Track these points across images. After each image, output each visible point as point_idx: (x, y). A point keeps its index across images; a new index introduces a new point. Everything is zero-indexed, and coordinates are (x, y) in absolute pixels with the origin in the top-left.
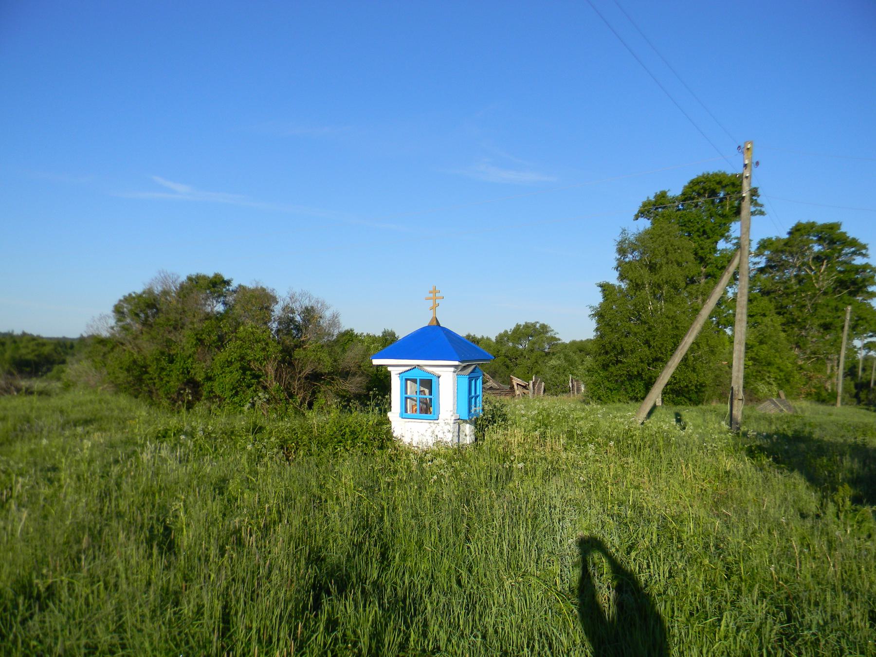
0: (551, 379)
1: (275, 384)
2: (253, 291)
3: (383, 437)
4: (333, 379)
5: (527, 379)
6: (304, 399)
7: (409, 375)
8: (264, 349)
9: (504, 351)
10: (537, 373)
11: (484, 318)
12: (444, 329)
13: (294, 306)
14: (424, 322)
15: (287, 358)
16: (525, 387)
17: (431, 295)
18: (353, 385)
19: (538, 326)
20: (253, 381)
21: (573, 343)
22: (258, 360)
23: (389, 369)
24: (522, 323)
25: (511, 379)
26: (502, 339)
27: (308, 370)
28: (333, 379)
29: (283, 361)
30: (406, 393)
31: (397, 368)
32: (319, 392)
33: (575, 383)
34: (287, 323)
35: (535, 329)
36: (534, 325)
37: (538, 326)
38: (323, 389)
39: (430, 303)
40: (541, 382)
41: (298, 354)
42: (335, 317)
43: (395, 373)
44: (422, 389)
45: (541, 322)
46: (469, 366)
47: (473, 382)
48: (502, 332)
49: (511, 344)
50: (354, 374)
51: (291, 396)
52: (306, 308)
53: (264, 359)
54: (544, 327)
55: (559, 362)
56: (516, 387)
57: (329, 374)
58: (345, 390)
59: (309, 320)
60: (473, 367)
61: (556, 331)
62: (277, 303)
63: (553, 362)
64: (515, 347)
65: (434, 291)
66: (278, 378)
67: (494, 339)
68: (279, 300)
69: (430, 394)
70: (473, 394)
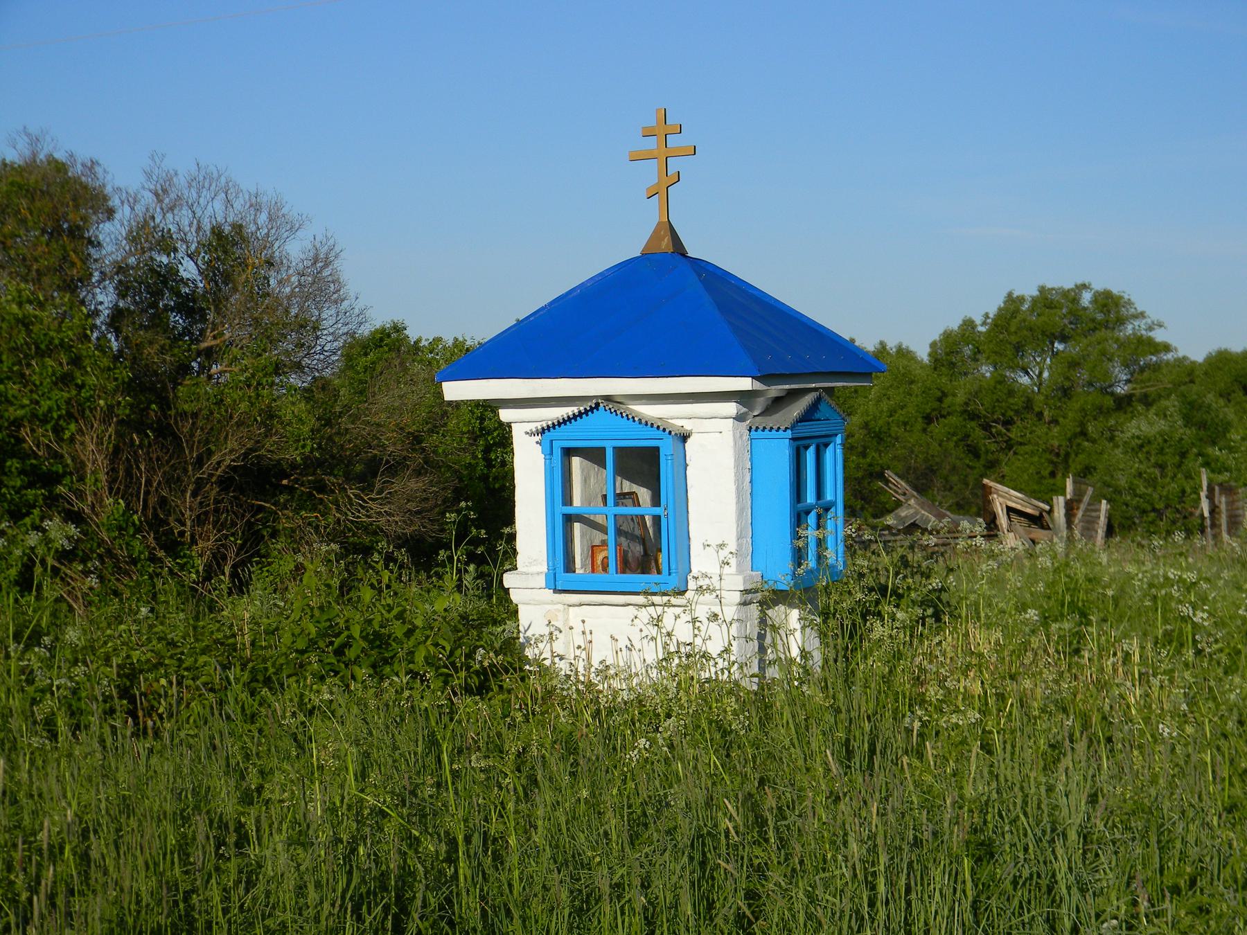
0: (1132, 489)
1: (113, 506)
2: (21, 170)
3: (487, 658)
4: (322, 488)
5: (1043, 488)
6: (218, 558)
7: (578, 435)
8: (65, 380)
9: (961, 398)
10: (1085, 473)
11: (900, 289)
12: (714, 279)
13: (169, 223)
14: (630, 244)
15: (151, 410)
16: (1038, 521)
17: (651, 143)
18: (391, 508)
19: (1086, 298)
20: (30, 493)
21: (1221, 360)
22: (44, 420)
23: (505, 415)
24: (1028, 290)
25: (987, 491)
26: (954, 350)
27: (227, 453)
28: (322, 488)
29: (137, 423)
30: (568, 499)
31: (531, 413)
32: (274, 534)
33: (1222, 501)
34: (151, 287)
35: (1076, 314)
36: (1072, 296)
37: (1086, 298)
38: (284, 524)
39: (649, 172)
40: (1096, 499)
41: (189, 396)
42: (321, 261)
43: (523, 428)
44: (627, 486)
45: (1098, 286)
46: (793, 395)
47: (810, 455)
48: (955, 324)
49: (986, 370)
50: (395, 468)
51: (172, 546)
52: (217, 232)
53: (70, 416)
54: (1109, 304)
55: (1162, 425)
56: (1003, 520)
57: (310, 464)
58: (366, 528)
59: (227, 278)
60: (808, 400)
61: (1153, 315)
62: (110, 213)
63: (1141, 425)
64: (1001, 381)
65: (663, 129)
66: (122, 482)
67: (923, 353)
68: (115, 202)
69: (656, 501)
70: (810, 498)
